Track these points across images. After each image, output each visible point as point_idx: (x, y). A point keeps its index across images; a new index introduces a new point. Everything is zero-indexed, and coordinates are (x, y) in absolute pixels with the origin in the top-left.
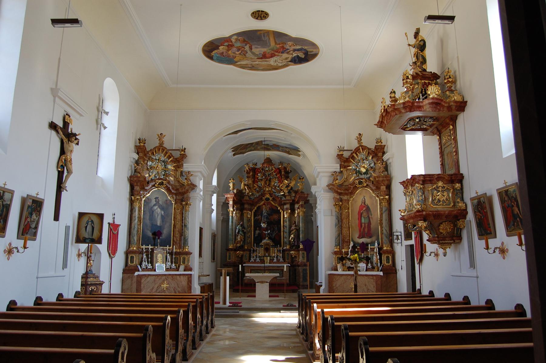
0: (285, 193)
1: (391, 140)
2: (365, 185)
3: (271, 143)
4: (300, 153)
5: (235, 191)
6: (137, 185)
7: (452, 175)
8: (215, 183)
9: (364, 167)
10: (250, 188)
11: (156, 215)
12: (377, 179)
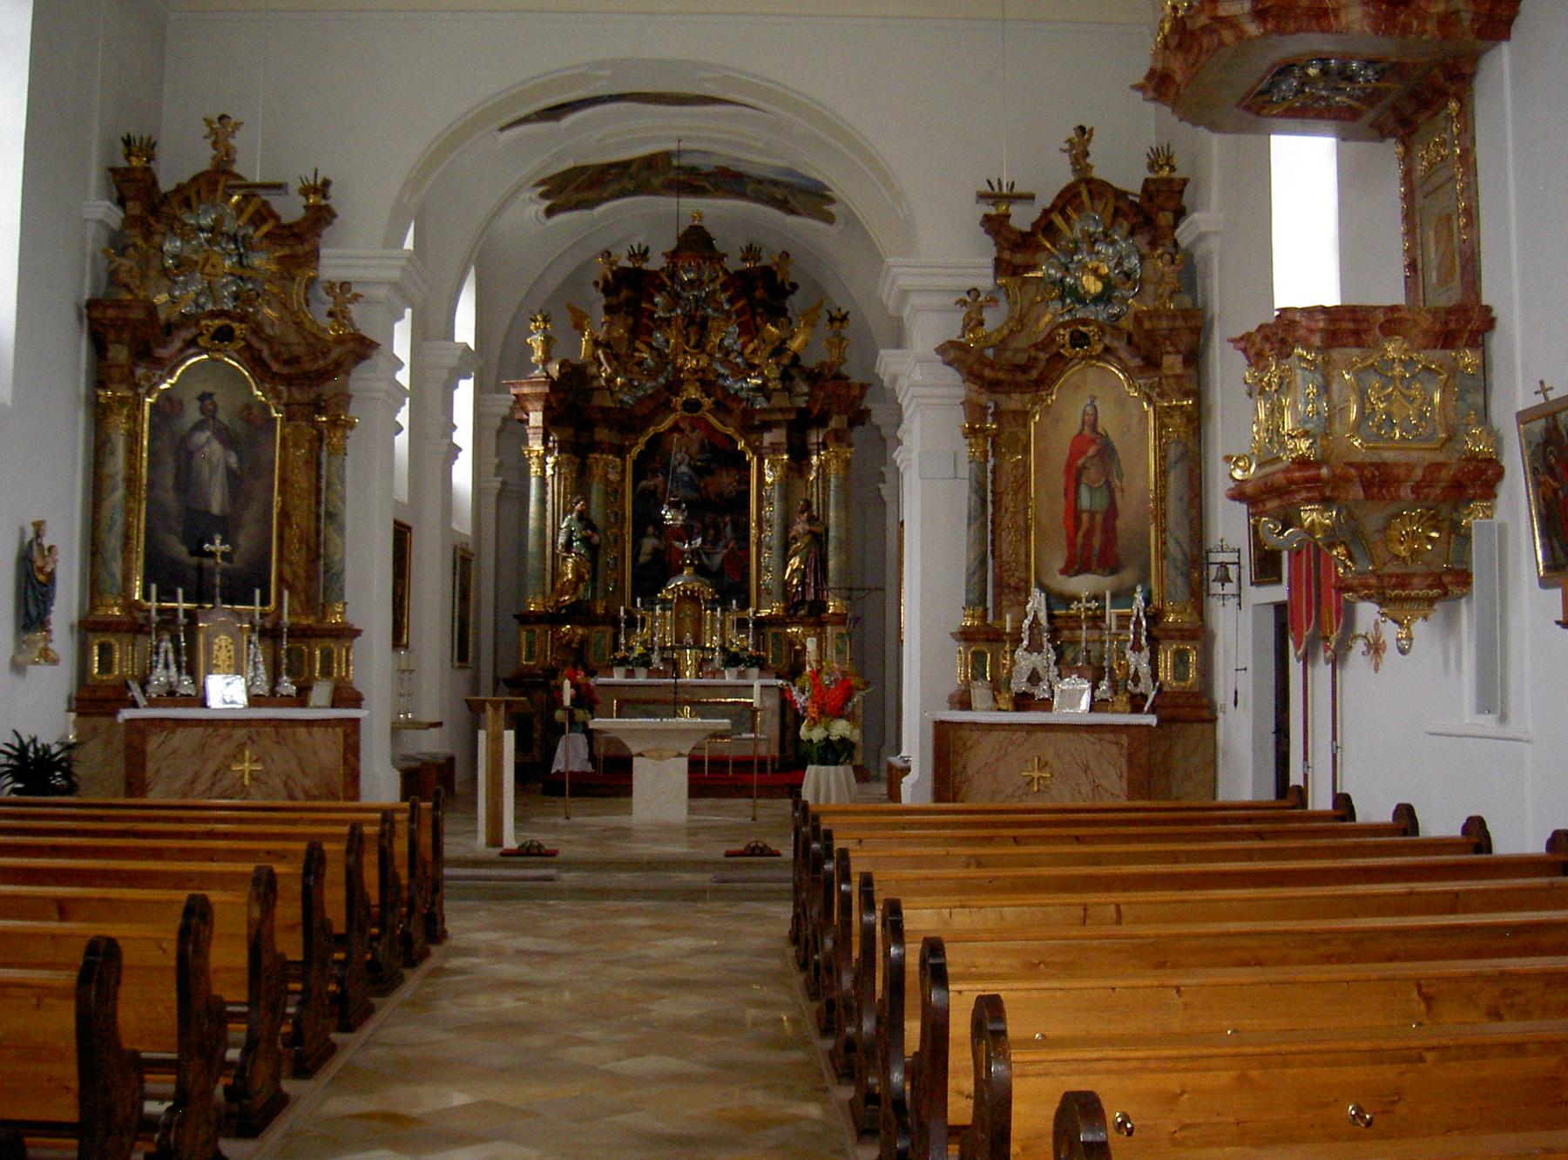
0: (766, 380)
1: (1210, 154)
2: (1099, 348)
3: (706, 164)
4: (833, 209)
5: (554, 369)
6: (119, 342)
7: (1449, 311)
8: (465, 330)
9: (1095, 272)
10: (617, 357)
11: (206, 473)
12: (1147, 325)
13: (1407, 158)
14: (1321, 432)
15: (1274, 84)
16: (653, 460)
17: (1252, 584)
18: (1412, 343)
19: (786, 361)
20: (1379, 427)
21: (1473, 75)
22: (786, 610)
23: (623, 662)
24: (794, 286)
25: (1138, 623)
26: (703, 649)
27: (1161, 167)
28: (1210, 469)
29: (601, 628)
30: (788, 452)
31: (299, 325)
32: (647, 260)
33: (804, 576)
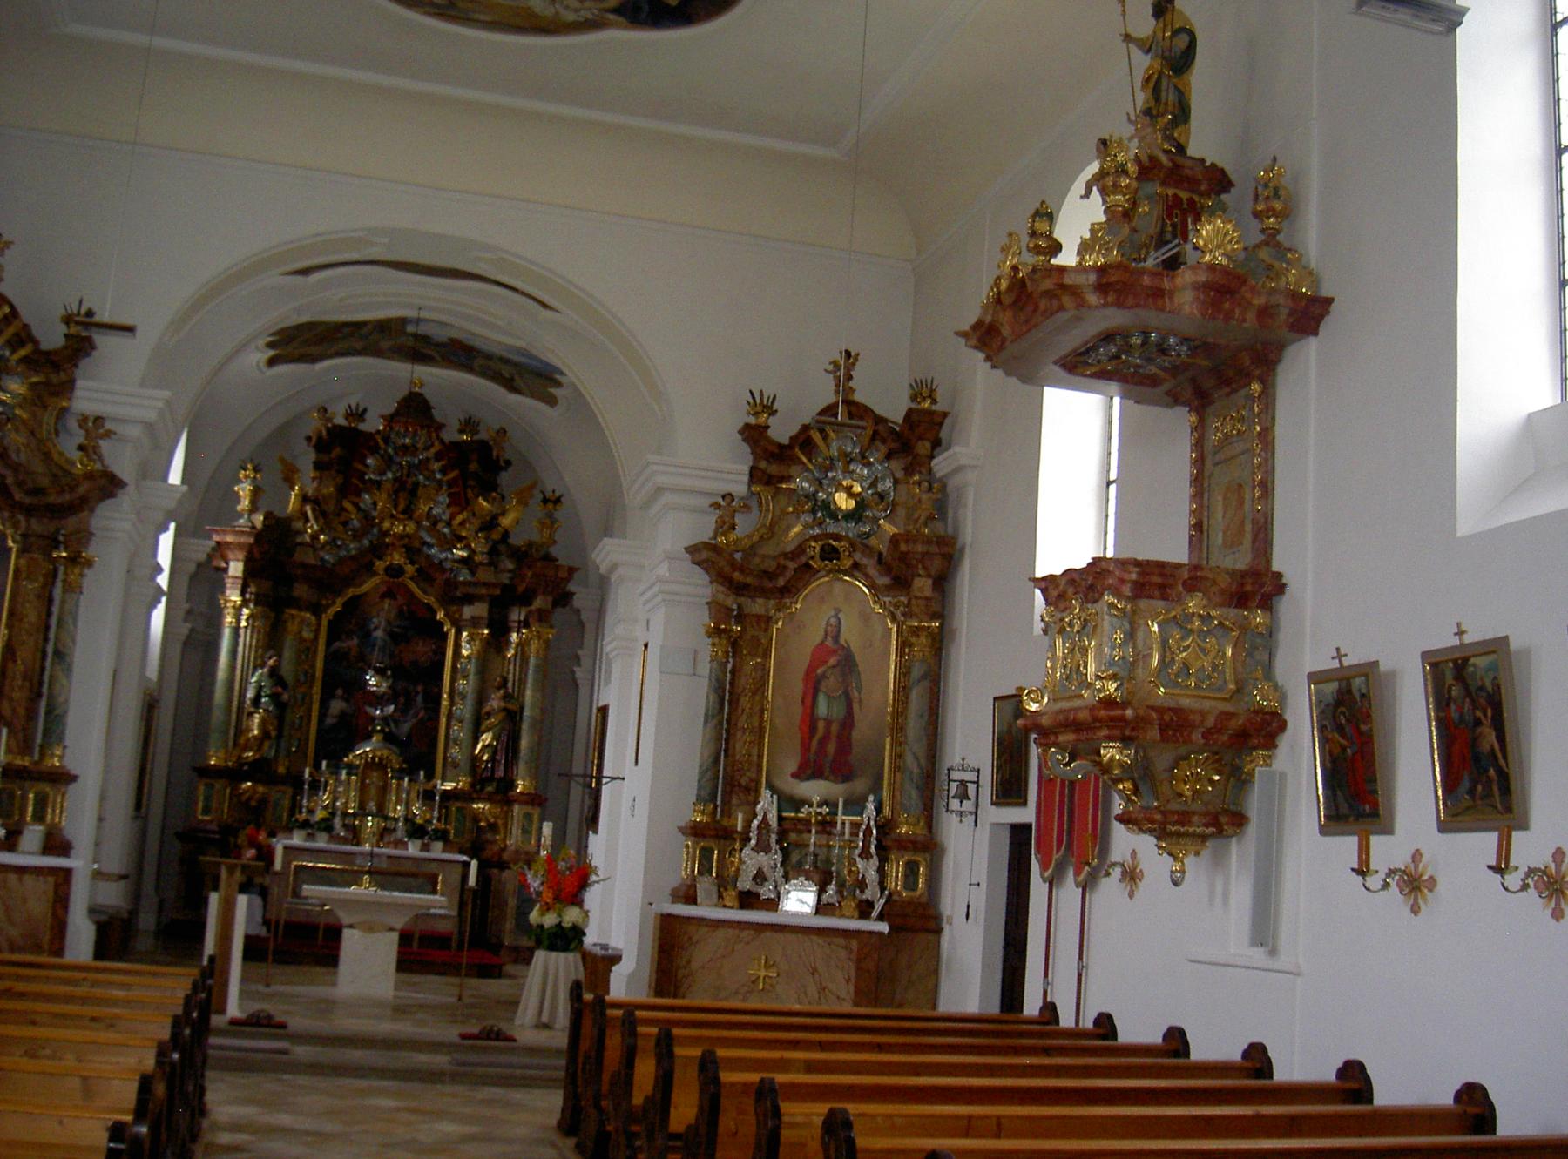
0: (473, 552)
2: (848, 563)
3: (441, 335)
5: (259, 519)
7: (1243, 574)
9: (848, 491)
12: (903, 547)
13: (1200, 429)
14: (1125, 672)
15: (1094, 348)
16: (352, 619)
17: (993, 804)
18: (1209, 599)
19: (495, 536)
20: (1177, 675)
21: (1278, 361)
22: (473, 785)
23: (305, 825)
24: (508, 463)
25: (868, 832)
26: (386, 818)
27: (924, 399)
28: (950, 691)
29: (283, 788)
30: (488, 627)
31: (47, 456)
32: (364, 421)
33: (495, 752)
